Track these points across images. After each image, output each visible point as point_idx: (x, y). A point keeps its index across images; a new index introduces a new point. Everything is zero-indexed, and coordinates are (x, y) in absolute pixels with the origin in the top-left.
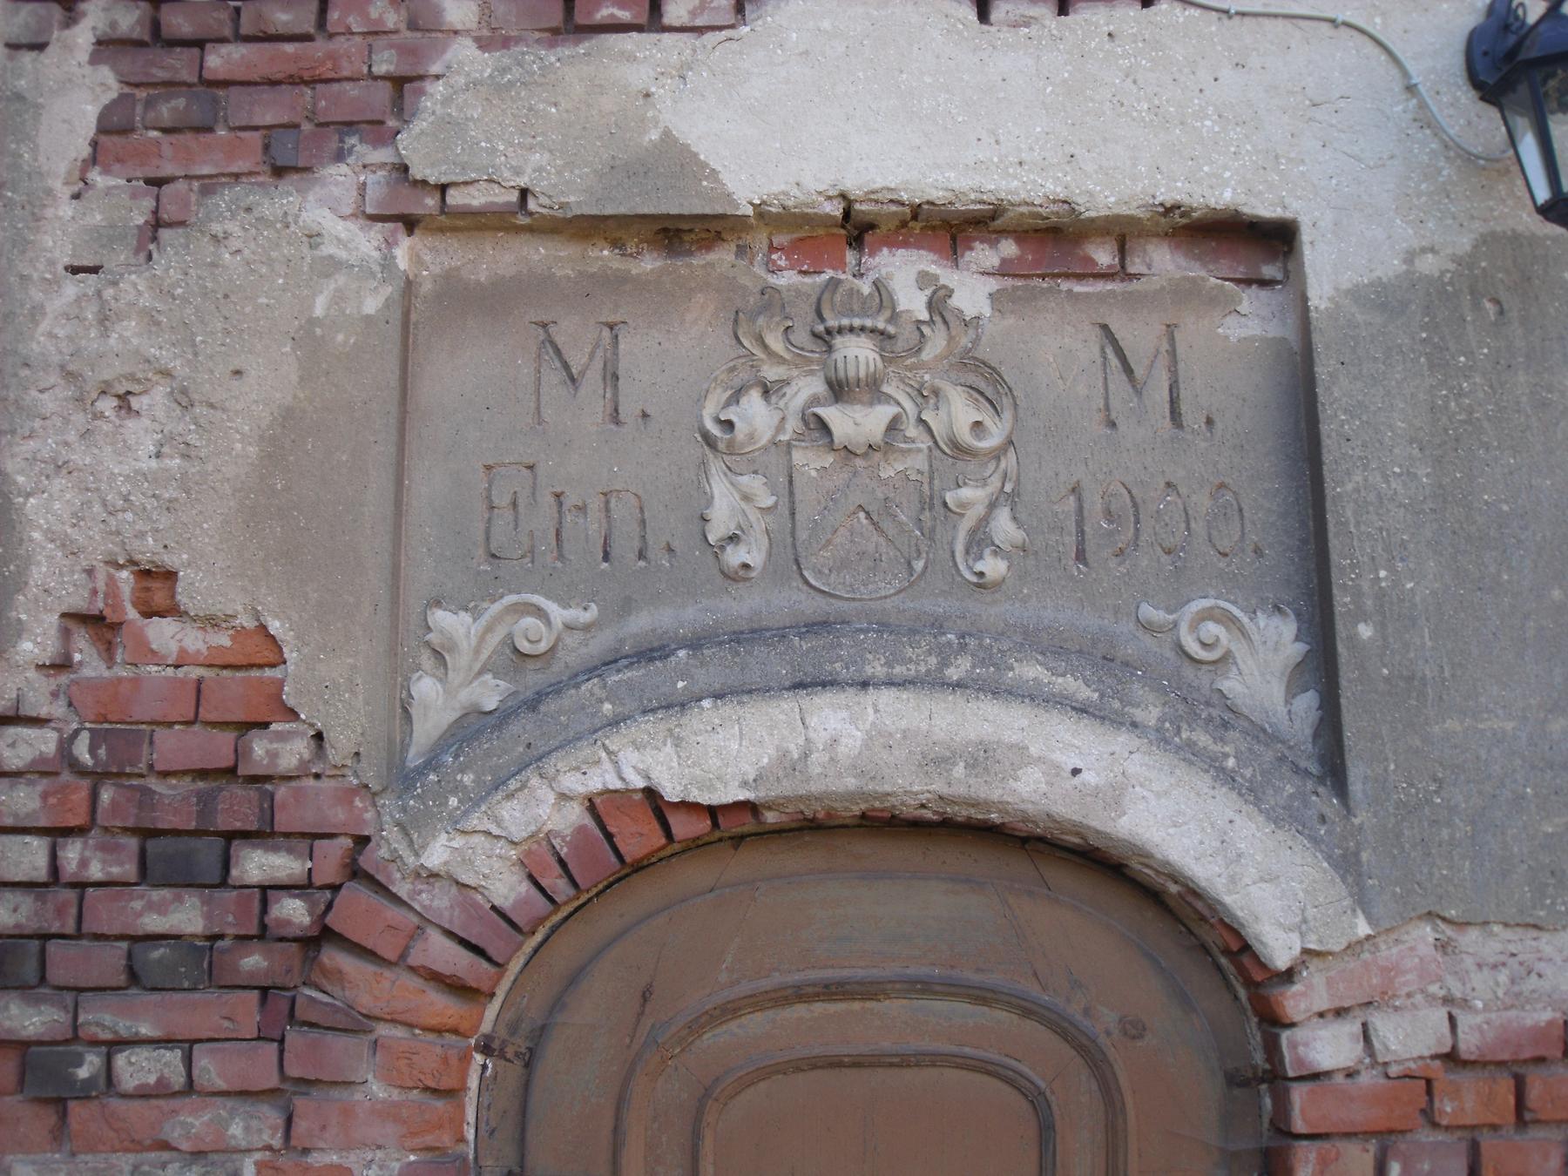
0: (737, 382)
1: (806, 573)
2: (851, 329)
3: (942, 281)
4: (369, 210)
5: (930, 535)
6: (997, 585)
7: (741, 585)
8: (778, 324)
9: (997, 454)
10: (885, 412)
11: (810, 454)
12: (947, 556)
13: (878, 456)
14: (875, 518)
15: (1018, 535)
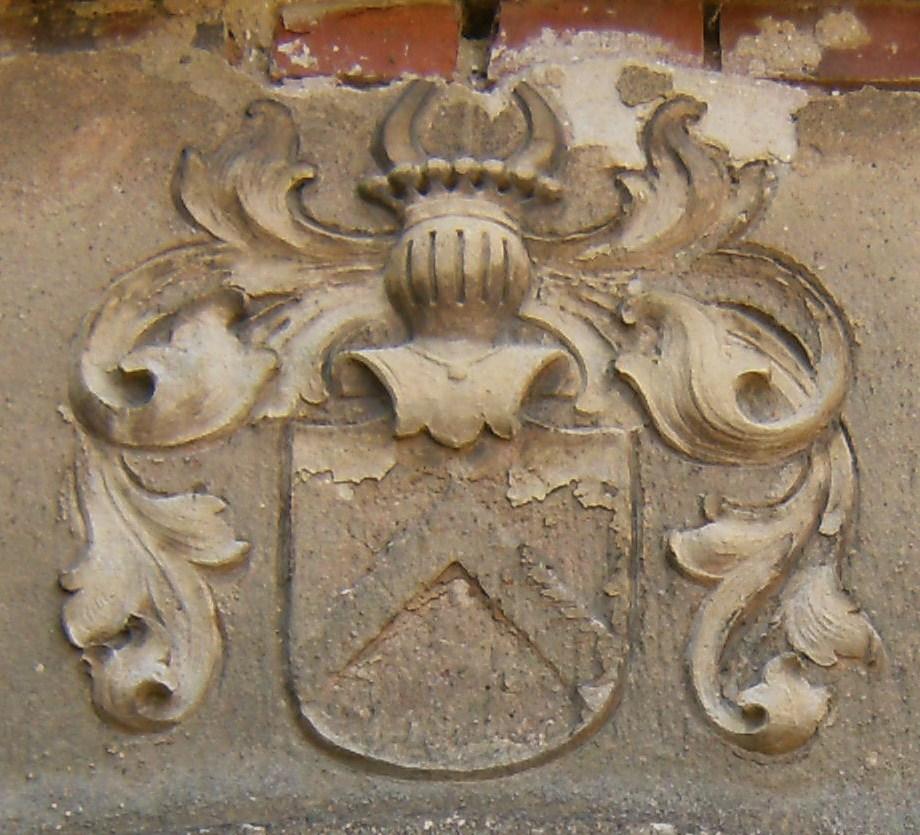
0: (172, 298)
1: (309, 713)
2: (453, 181)
3: (679, 88)
4: (286, 15)
5: (633, 631)
6: (796, 743)
7: (140, 740)
8: (279, 173)
9: (804, 448)
10: (519, 362)
11: (338, 450)
12: (673, 676)
13: (505, 455)
14: (493, 591)
15: (854, 629)
